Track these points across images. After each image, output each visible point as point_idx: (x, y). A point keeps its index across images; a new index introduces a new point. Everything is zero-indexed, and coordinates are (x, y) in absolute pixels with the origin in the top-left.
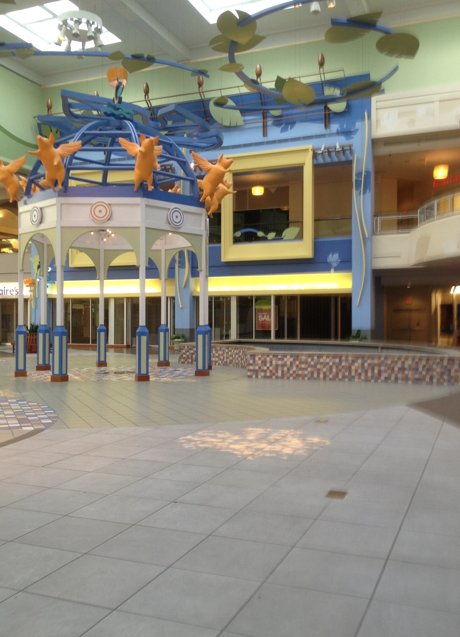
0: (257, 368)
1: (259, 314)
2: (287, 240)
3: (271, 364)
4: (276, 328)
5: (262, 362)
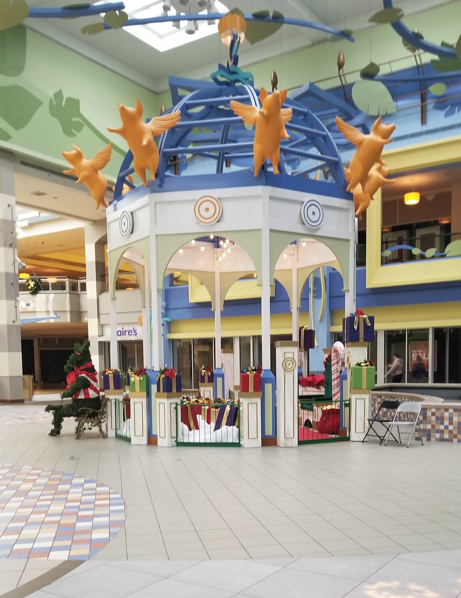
0: (429, 427)
1: (413, 351)
2: (450, 257)
3: (451, 423)
4: (435, 368)
5: (437, 418)
